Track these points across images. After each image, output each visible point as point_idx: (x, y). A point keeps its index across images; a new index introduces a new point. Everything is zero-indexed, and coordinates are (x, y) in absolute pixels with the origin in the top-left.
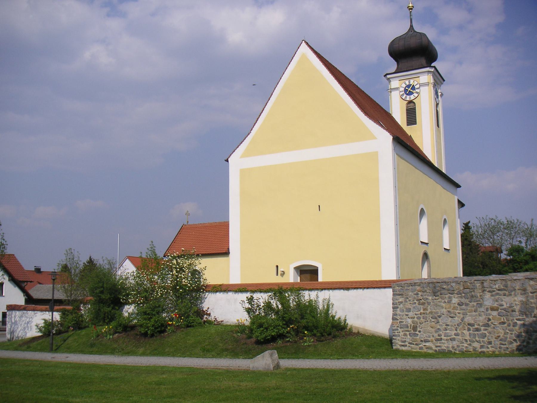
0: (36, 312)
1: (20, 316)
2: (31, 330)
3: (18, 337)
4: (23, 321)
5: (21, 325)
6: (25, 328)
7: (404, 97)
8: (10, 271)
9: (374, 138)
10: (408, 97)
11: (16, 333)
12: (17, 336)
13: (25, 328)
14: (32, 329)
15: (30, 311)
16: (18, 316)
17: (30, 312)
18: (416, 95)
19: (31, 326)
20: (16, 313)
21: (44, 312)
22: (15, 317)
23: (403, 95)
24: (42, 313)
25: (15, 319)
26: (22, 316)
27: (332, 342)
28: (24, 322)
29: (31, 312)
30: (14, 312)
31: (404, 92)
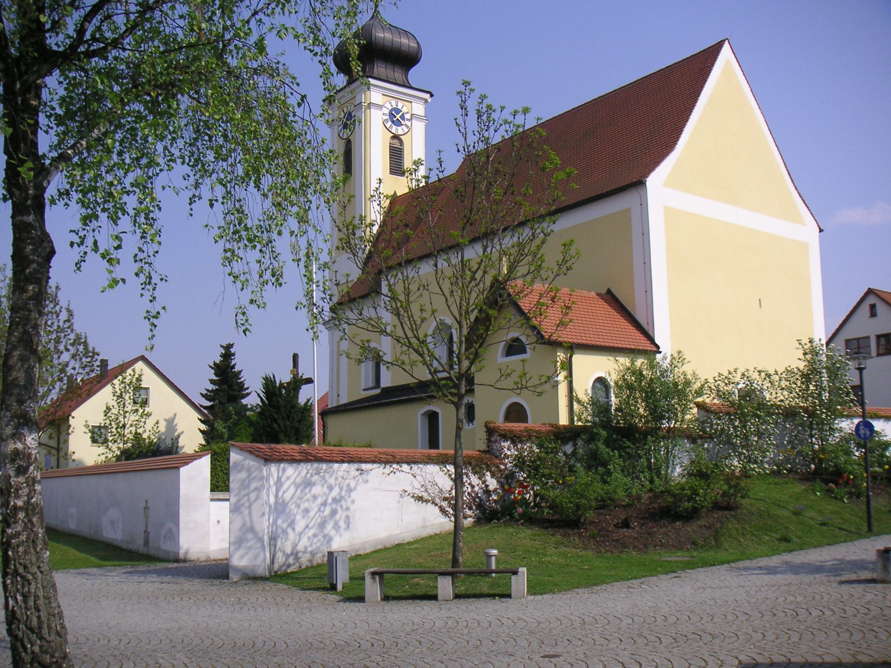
0: (364, 466)
1: (299, 480)
2: (348, 527)
3: (295, 554)
4: (315, 497)
5: (307, 511)
6: (322, 525)
7: (388, 125)
8: (624, 321)
9: (667, 210)
10: (394, 127)
11: (287, 539)
12: (288, 550)
13: (322, 525)
14: (351, 526)
15: (343, 462)
16: (294, 483)
17: (342, 469)
18: (406, 130)
19: (347, 517)
20: (284, 470)
21: (395, 466)
22: (279, 483)
23: (386, 120)
24: (388, 469)
25: (277, 491)
26: (308, 484)
27: (598, 477)
28: (319, 501)
29: (345, 465)
30: (273, 468)
31: (388, 117)
